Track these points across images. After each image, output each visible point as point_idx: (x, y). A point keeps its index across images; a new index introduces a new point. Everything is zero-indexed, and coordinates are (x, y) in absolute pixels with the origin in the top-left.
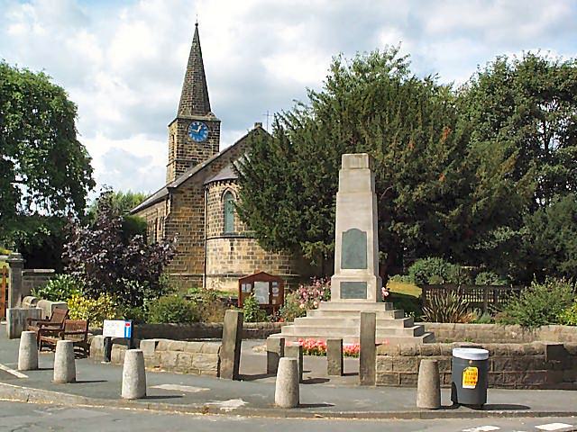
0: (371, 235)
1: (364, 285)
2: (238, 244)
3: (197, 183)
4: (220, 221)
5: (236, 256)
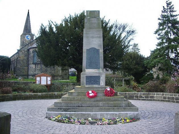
0: (101, 51)
2: (37, 66)
3: (26, 49)
4: (32, 59)
5: (37, 69)
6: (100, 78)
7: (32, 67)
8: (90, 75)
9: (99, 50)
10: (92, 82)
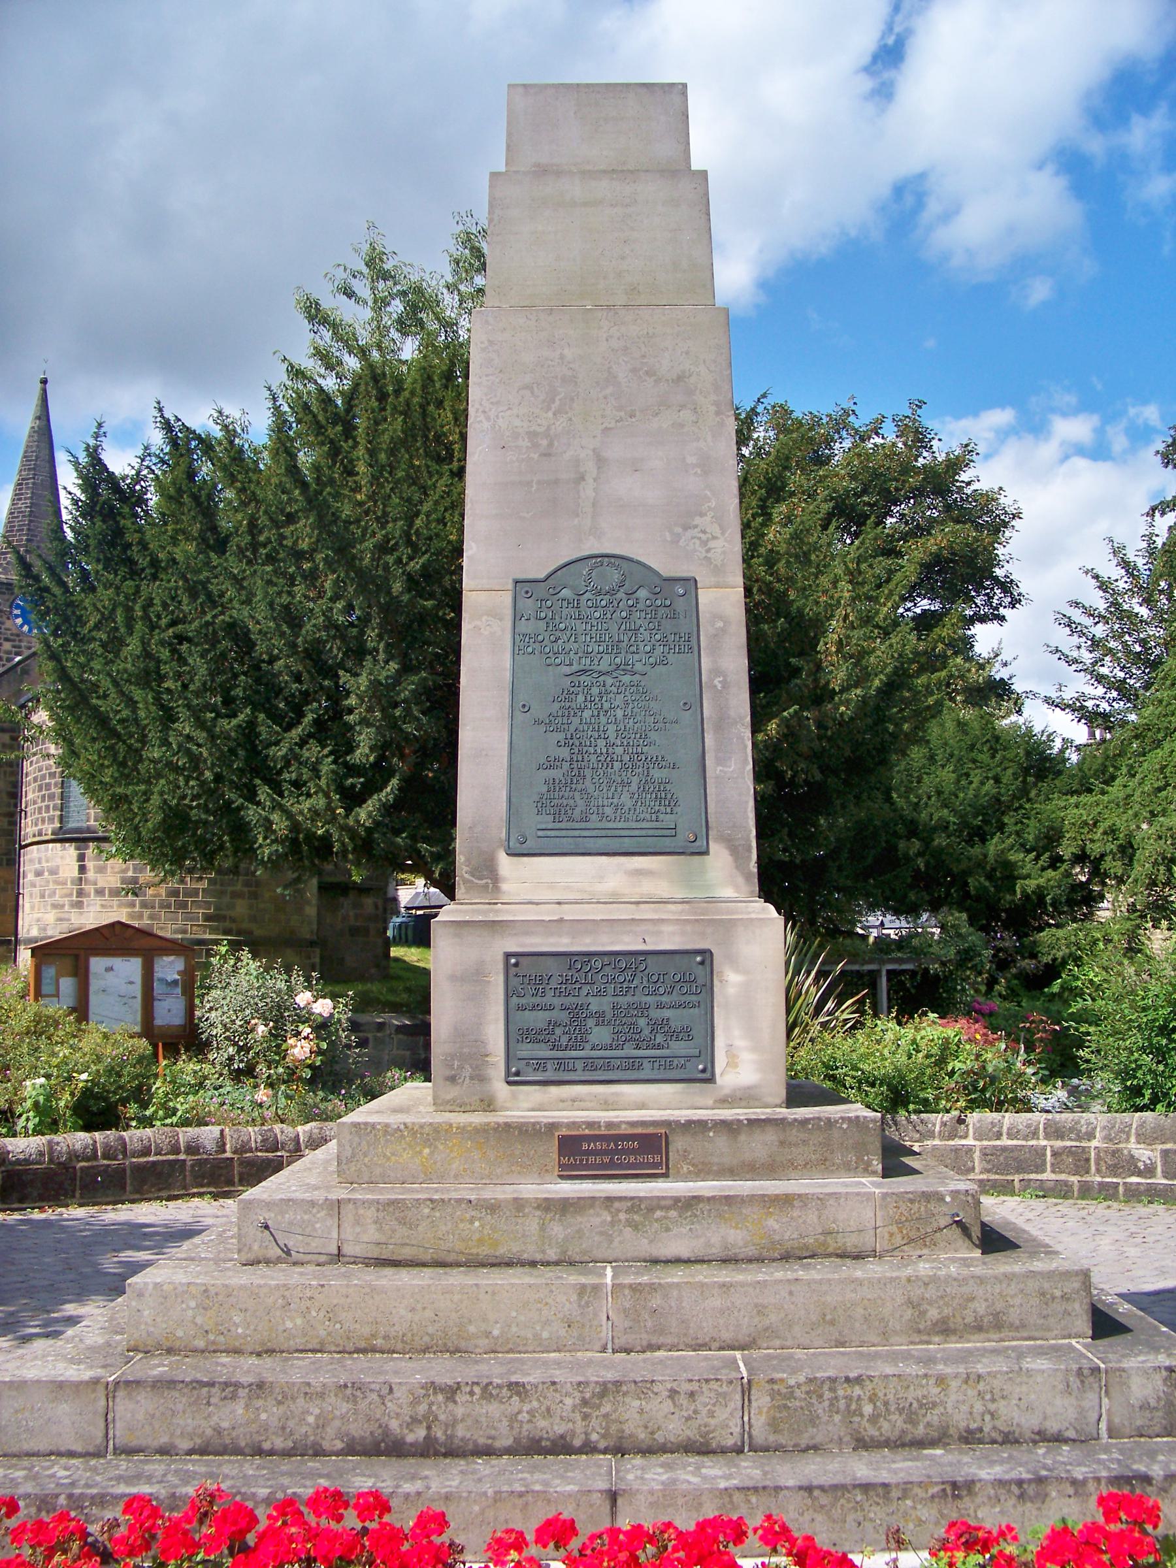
1: (688, 976)
5: (90, 889)
6: (708, 989)
7: (54, 872)
8: (564, 944)
9: (691, 583)
10: (600, 1034)
